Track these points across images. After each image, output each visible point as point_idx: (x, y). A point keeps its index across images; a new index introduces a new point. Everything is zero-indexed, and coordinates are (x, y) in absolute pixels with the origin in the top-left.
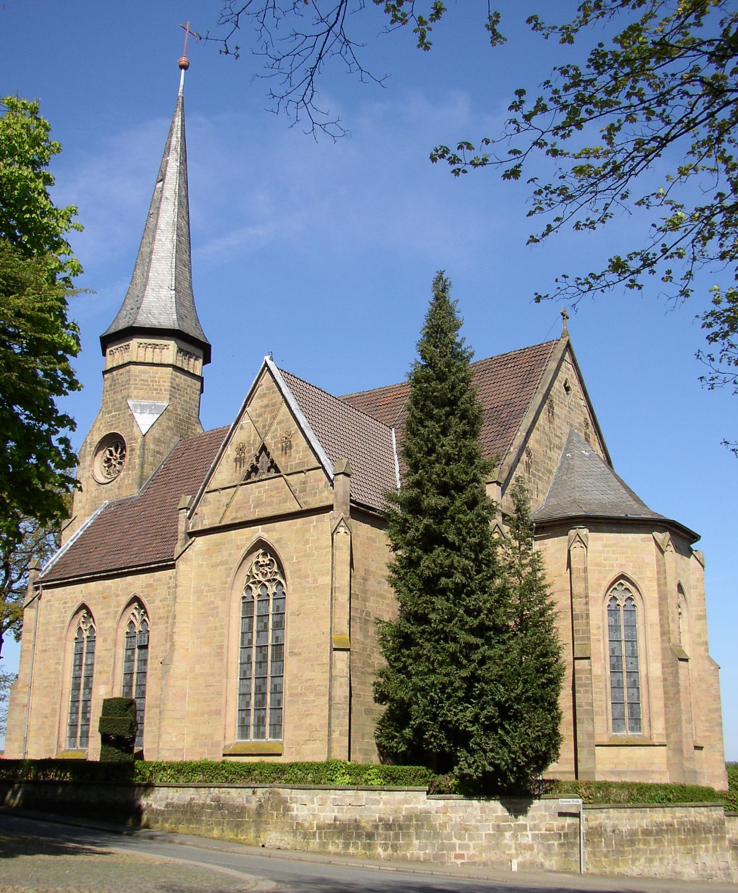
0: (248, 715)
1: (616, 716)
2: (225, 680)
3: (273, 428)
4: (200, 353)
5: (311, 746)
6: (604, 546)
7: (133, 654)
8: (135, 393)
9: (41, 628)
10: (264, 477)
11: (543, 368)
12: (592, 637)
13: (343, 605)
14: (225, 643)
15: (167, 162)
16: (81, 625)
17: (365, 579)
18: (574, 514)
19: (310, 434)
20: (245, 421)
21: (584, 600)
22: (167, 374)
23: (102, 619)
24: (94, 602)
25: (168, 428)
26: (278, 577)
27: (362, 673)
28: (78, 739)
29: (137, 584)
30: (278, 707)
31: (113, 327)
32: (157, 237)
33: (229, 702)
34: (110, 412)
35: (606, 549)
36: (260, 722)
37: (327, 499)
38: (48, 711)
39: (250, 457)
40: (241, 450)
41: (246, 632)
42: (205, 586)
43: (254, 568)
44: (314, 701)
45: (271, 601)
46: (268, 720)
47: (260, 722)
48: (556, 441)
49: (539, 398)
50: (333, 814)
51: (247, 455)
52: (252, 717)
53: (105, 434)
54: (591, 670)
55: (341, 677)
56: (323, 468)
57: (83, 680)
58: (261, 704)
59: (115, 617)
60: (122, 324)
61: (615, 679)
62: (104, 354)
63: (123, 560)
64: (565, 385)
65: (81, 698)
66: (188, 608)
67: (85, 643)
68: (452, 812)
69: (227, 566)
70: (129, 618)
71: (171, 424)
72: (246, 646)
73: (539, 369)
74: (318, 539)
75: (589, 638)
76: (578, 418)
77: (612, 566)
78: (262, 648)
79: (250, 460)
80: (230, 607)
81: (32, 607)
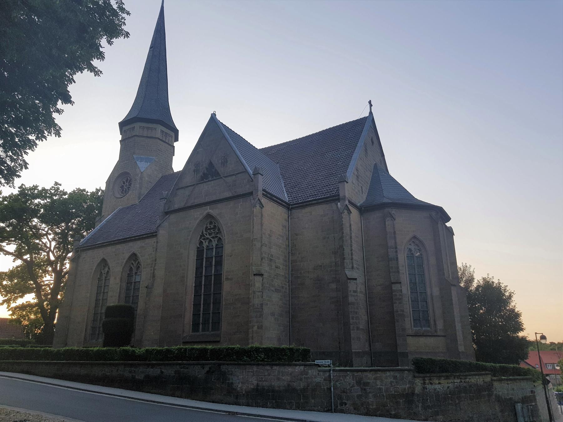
17: (270, 236)
45: (214, 249)
47: (206, 322)
52: (201, 319)
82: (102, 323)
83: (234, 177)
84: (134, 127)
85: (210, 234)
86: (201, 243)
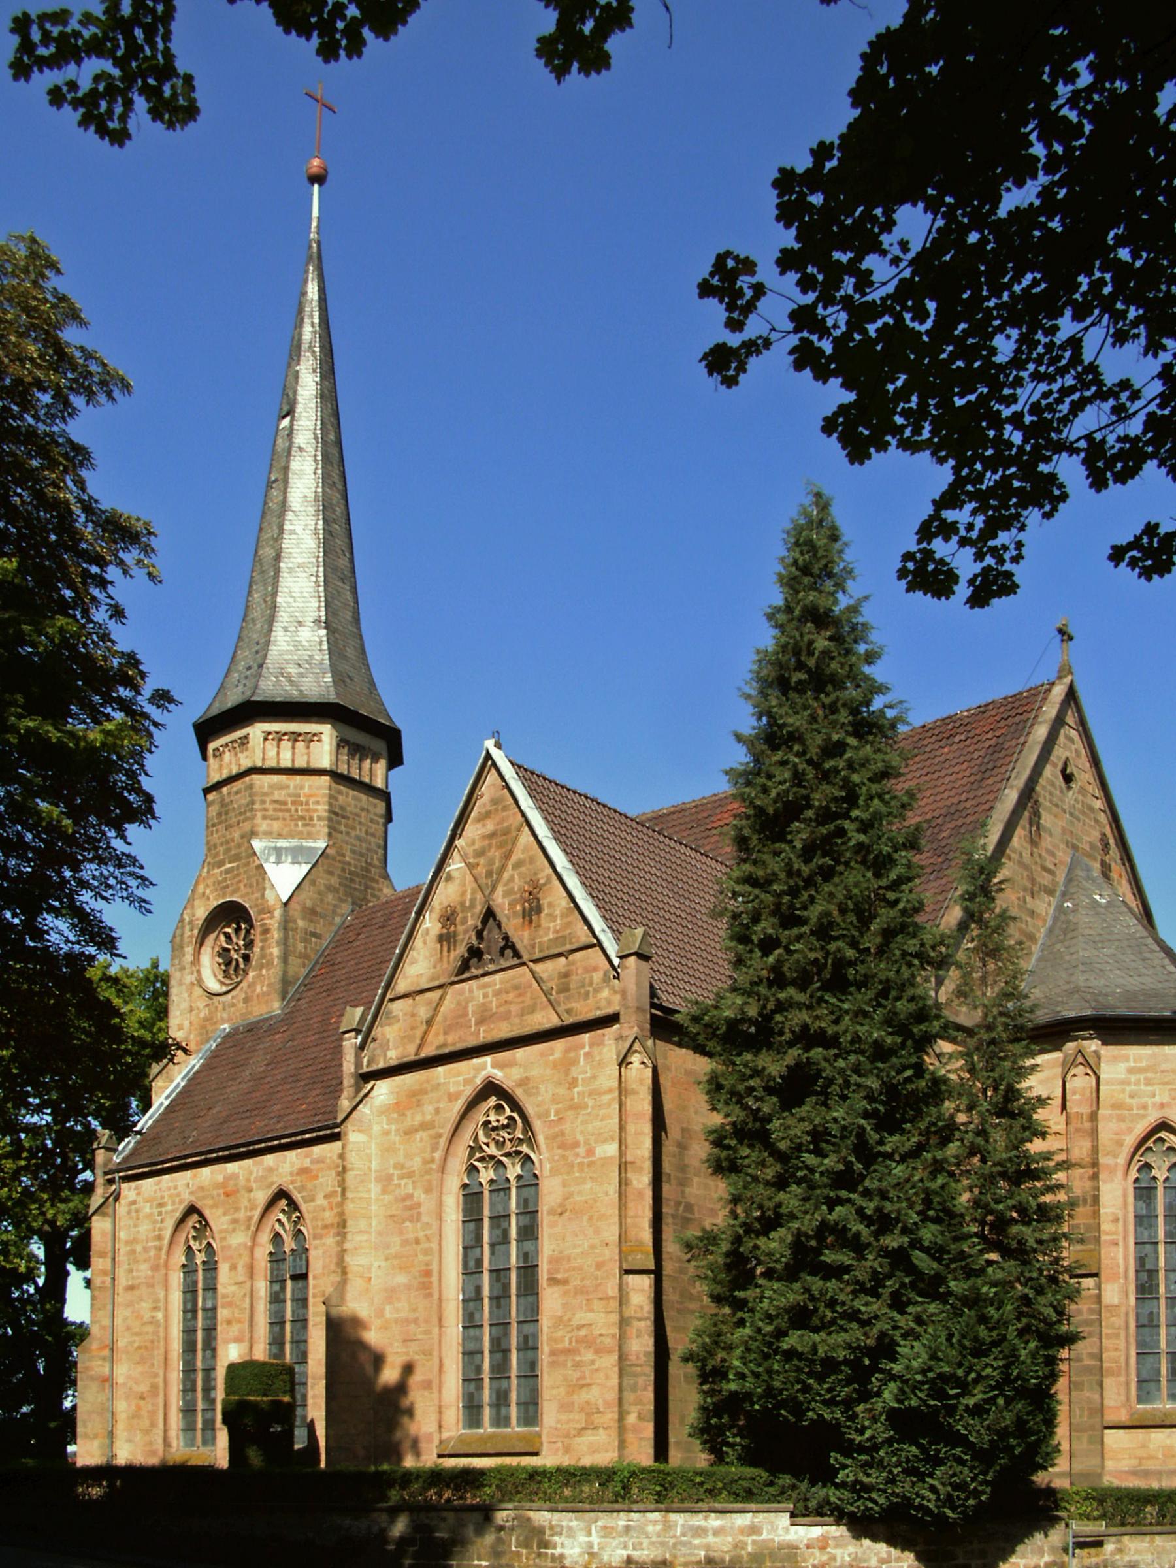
0: (480, 1388)
1: (1144, 1376)
2: (436, 1330)
3: (506, 875)
4: (380, 745)
5: (589, 1438)
6: (1131, 1071)
7: (283, 1289)
8: (263, 826)
9: (123, 1250)
10: (491, 967)
11: (1022, 740)
12: (1103, 1238)
13: (640, 1194)
14: (435, 1267)
15: (296, 375)
16: (192, 1243)
18: (1073, 1014)
19: (573, 882)
20: (455, 865)
21: (1090, 1171)
22: (319, 788)
23: (226, 1231)
24: (210, 1202)
25: (330, 888)
26: (524, 1148)
27: (679, 1311)
28: (199, 1433)
29: (283, 1167)
30: (530, 1374)
31: (217, 704)
32: (287, 527)
33: (445, 1368)
34: (221, 864)
35: (1133, 1078)
36: (501, 1399)
37: (609, 1003)
38: (143, 1388)
39: (466, 931)
40: (448, 918)
41: (471, 1246)
42: (396, 1166)
43: (481, 1133)
44: (593, 1362)
45: (514, 1191)
46: (514, 1396)
47: (501, 1399)
48: (1045, 879)
49: (1011, 796)
50: (625, 1553)
51: (460, 928)
53: (216, 904)
54: (1099, 1296)
55: (640, 1320)
56: (600, 944)
57: (200, 1335)
58: (500, 1370)
59: (248, 1228)
60: (233, 698)
61: (1145, 1311)
62: (205, 758)
63: (257, 1128)
64: (1063, 771)
65: (199, 1364)
66: (370, 1204)
67: (200, 1272)
68: (836, 1546)
69: (432, 1132)
70: (273, 1229)
71: (334, 881)
72: (471, 1269)
73: (1013, 743)
74: (594, 1077)
75: (1097, 1240)
76: (1089, 835)
77: (1145, 1107)
78: (499, 1274)
79: (466, 937)
80: (440, 1204)
81: (105, 1215)
82: (77, 510)
83: (563, 959)
84: (246, 737)
85: (500, 1145)
86: (472, 1170)
